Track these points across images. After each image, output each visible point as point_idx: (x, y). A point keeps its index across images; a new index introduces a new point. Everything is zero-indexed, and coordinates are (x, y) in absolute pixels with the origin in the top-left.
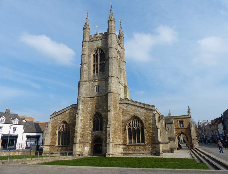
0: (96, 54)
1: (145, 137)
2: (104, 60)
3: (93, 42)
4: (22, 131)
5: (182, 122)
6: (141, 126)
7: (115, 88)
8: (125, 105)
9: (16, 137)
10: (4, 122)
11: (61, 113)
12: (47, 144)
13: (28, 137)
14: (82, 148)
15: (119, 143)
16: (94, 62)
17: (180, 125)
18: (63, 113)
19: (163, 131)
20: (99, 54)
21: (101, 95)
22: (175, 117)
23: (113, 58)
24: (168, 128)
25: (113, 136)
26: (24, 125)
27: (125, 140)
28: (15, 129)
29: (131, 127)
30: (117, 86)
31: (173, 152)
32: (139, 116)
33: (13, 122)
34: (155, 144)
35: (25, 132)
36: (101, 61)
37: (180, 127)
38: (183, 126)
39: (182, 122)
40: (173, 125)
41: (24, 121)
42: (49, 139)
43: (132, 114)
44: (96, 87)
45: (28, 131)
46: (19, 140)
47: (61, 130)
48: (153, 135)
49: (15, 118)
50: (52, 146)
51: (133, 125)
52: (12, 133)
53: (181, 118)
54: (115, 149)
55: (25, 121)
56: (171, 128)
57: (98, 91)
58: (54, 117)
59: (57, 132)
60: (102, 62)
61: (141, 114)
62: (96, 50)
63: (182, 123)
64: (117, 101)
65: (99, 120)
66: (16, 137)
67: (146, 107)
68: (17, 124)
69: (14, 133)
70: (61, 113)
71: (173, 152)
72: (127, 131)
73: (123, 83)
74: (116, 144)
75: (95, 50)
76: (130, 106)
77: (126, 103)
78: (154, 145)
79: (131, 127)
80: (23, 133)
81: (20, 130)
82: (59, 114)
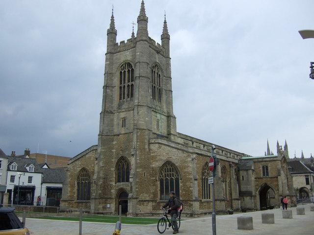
0: (123, 72)
1: (180, 191)
2: (132, 81)
3: (119, 54)
4: (40, 182)
5: (265, 169)
6: (176, 176)
7: (143, 122)
8: (157, 145)
9: (32, 189)
10: (16, 170)
11: (81, 158)
12: (65, 199)
13: (48, 189)
14: (104, 205)
15: (148, 199)
16: (121, 83)
17: (264, 173)
18: (82, 157)
19: (217, 183)
20: (127, 70)
21: (128, 131)
22: (256, 160)
23: (141, 78)
24: (243, 176)
25: (137, 190)
26: (42, 173)
27: (155, 195)
28: (30, 179)
29: (163, 176)
30: (147, 119)
31: (304, 214)
32: (174, 161)
33: (28, 168)
34: (192, 201)
35: (43, 182)
36: (129, 82)
37: (264, 175)
38: (268, 175)
39: (267, 167)
40: (250, 172)
41: (45, 167)
42: (69, 192)
43: (165, 158)
44: (122, 120)
45: (48, 181)
46: (37, 194)
47: (164, 176)
48: (191, 189)
49: (30, 164)
50: (71, 202)
51: (165, 175)
52: (26, 184)
53: (266, 161)
54: (139, 207)
55: (47, 167)
56: (248, 177)
57: (125, 126)
58: (73, 162)
59: (76, 183)
60: (130, 84)
61: (176, 157)
62: (123, 65)
63: (267, 169)
64: (146, 141)
65: (125, 167)
66: (32, 189)
67: (78, 157)
68: (33, 171)
69: (30, 184)
70: (81, 158)
71: (304, 214)
72: (159, 183)
73: (165, 110)
74: (142, 201)
75: (122, 66)
76: (163, 146)
77: (159, 143)
78: (191, 203)
79: (163, 176)
80: (42, 184)
81: (37, 179)
82: (206, 154)
